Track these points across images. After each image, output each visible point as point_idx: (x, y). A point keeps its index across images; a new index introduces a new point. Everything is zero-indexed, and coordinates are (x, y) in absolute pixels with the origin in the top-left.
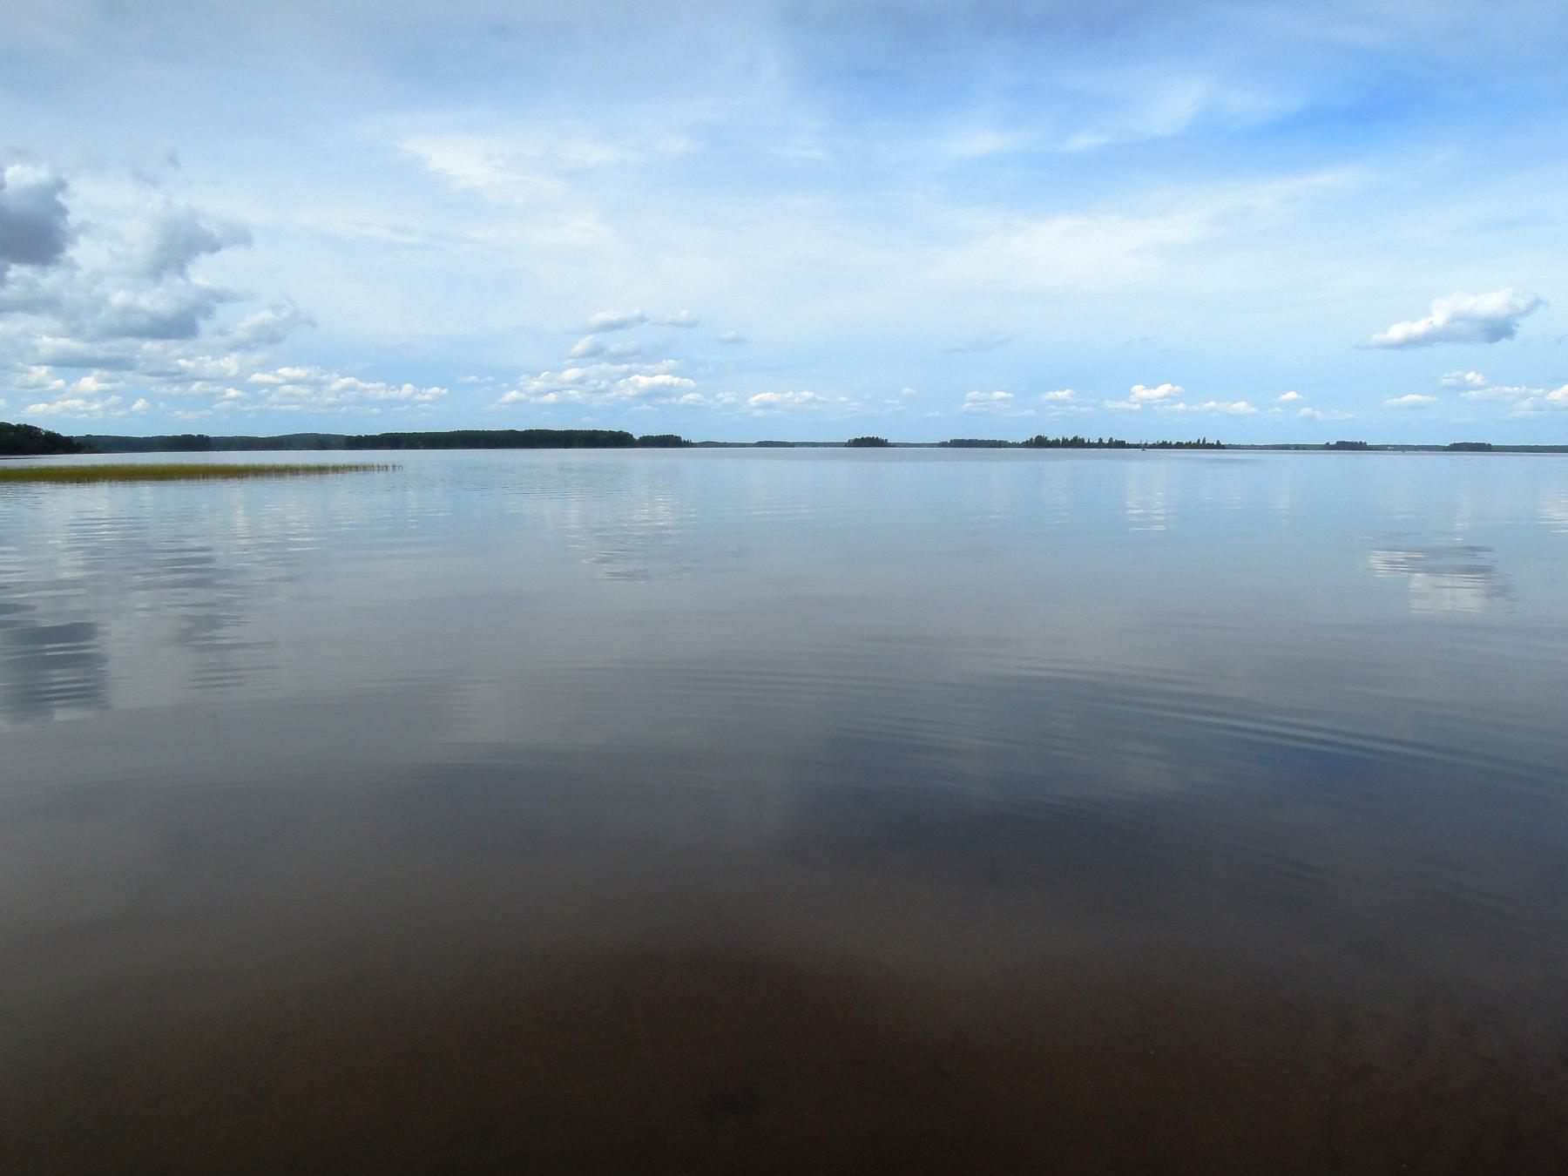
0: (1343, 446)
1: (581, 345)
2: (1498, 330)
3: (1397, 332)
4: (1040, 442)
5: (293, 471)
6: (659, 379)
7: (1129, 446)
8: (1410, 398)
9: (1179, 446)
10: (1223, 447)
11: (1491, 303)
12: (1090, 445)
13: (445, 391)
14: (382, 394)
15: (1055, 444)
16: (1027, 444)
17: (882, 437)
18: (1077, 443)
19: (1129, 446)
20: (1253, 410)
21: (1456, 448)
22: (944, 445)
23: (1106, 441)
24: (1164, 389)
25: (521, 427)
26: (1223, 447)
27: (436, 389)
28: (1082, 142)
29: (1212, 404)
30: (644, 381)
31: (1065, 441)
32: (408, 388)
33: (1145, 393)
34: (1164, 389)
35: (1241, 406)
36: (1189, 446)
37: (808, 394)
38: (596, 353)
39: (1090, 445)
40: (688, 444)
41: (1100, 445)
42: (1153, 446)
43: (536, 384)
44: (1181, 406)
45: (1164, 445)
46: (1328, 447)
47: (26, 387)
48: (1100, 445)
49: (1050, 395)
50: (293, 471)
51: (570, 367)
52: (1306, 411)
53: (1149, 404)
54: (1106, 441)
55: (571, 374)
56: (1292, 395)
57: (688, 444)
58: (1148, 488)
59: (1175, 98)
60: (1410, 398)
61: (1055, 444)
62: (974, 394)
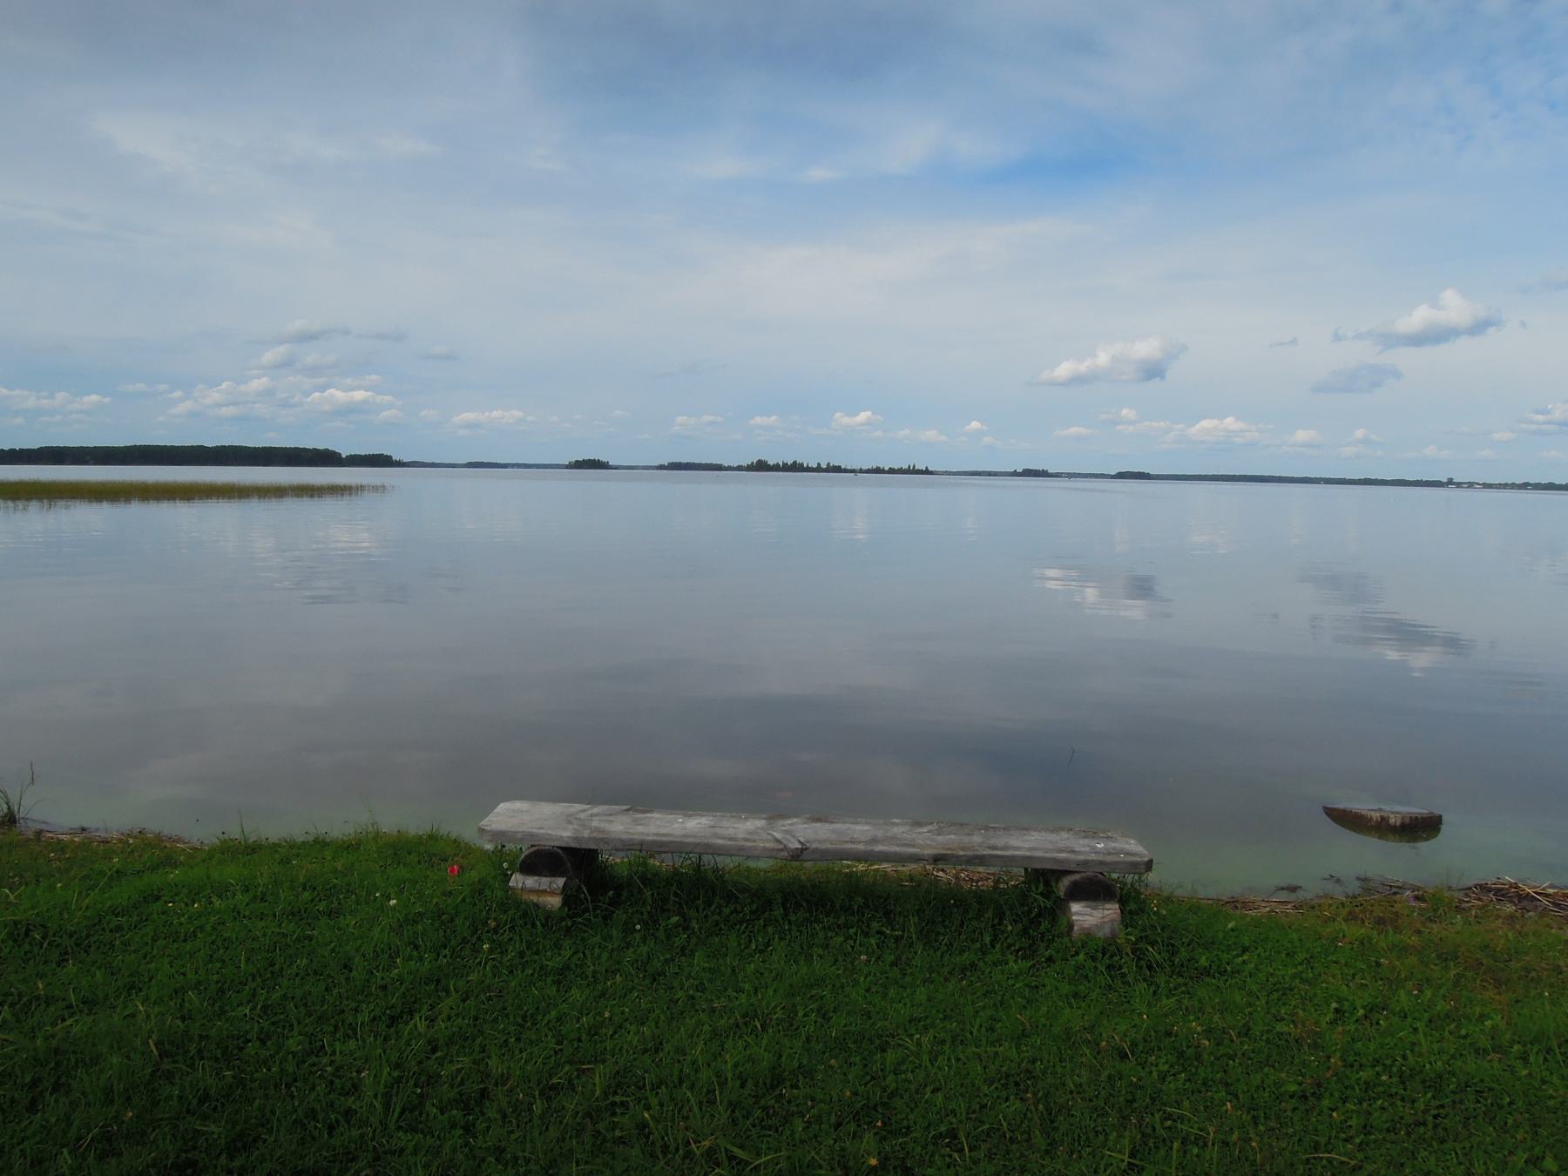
0: (1028, 473)
1: (270, 356)
2: (1153, 371)
3: (1064, 369)
4: (761, 466)
5: (278, 492)
6: (359, 395)
7: (846, 471)
8: (1074, 430)
9: (892, 471)
10: (931, 473)
11: (1145, 349)
12: (809, 470)
13: (107, 400)
14: (31, 403)
15: (776, 468)
16: (750, 468)
17: (603, 459)
18: (796, 467)
19: (846, 471)
20: (943, 438)
21: (1121, 476)
22: (661, 467)
23: (824, 466)
24: (863, 416)
25: (210, 443)
26: (931, 473)
27: (94, 398)
28: (818, 173)
29: (907, 431)
30: (340, 395)
31: (785, 465)
32: (61, 396)
33: (846, 420)
34: (863, 416)
35: (932, 434)
36: (901, 471)
37: (517, 414)
38: (287, 364)
39: (809, 470)
40: (399, 464)
41: (819, 469)
42: (868, 471)
43: (215, 396)
44: (879, 433)
45: (878, 471)
46: (1015, 474)
47: (987, 828)
48: (819, 469)
49: (758, 420)
50: (278, 492)
51: (259, 377)
52: (987, 440)
53: (854, 431)
54: (824, 466)
55: (257, 384)
56: (975, 425)
57: (399, 464)
58: (855, 510)
59: (909, 136)
60: (1074, 430)
61: (776, 468)
62: (681, 419)
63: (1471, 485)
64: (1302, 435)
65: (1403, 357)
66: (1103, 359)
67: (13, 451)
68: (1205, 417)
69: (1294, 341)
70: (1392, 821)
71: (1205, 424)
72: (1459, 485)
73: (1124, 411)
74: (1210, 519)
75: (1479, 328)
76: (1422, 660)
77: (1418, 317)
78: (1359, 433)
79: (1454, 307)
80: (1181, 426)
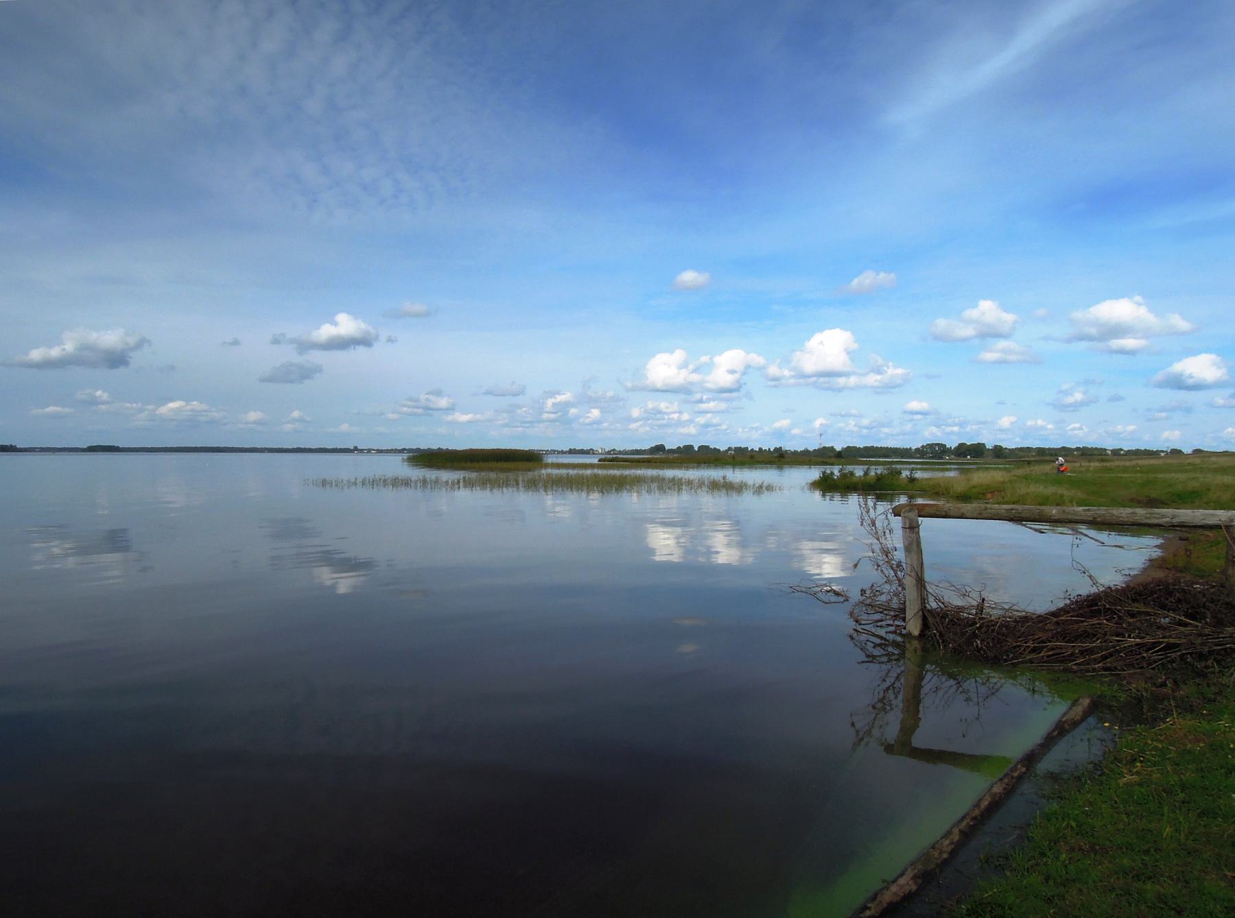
2: (116, 359)
3: (36, 355)
5: (572, 452)
8: (51, 409)
9: (380, 451)
11: (110, 338)
21: (92, 449)
25: (199, 445)
60: (51, 409)
63: (369, 451)
64: (253, 416)
65: (316, 357)
66: (69, 347)
67: (806, 453)
68: (171, 400)
69: (235, 343)
70: (798, 353)
71: (172, 405)
72: (362, 451)
73: (99, 393)
74: (172, 486)
75: (364, 341)
76: (345, 584)
77: (326, 331)
78: (296, 414)
79: (346, 325)
80: (151, 407)
